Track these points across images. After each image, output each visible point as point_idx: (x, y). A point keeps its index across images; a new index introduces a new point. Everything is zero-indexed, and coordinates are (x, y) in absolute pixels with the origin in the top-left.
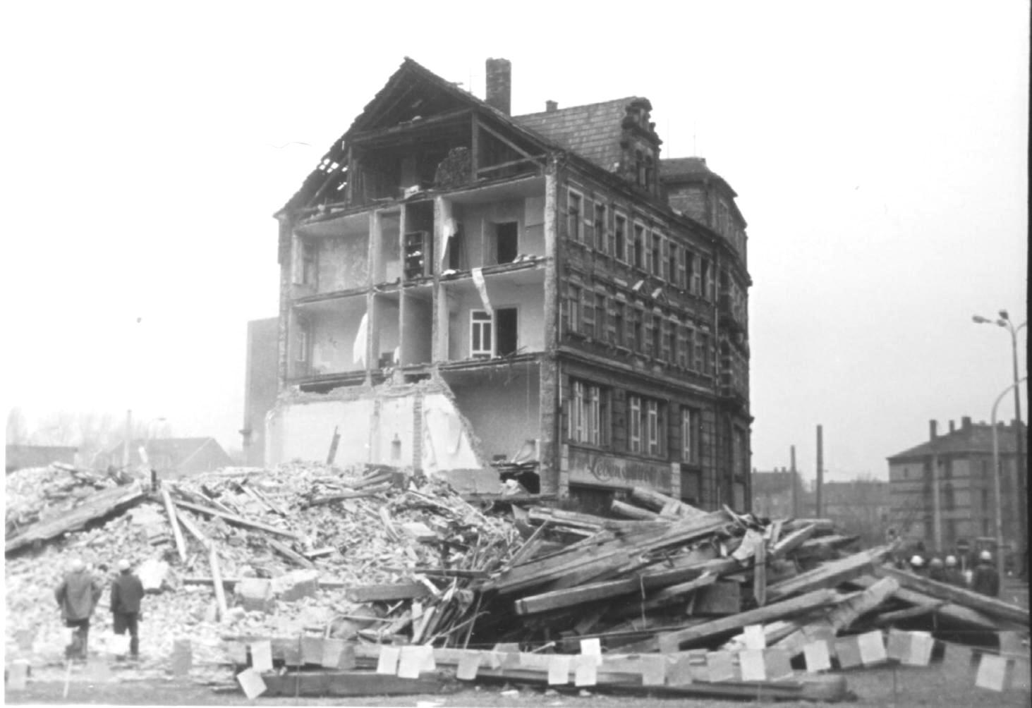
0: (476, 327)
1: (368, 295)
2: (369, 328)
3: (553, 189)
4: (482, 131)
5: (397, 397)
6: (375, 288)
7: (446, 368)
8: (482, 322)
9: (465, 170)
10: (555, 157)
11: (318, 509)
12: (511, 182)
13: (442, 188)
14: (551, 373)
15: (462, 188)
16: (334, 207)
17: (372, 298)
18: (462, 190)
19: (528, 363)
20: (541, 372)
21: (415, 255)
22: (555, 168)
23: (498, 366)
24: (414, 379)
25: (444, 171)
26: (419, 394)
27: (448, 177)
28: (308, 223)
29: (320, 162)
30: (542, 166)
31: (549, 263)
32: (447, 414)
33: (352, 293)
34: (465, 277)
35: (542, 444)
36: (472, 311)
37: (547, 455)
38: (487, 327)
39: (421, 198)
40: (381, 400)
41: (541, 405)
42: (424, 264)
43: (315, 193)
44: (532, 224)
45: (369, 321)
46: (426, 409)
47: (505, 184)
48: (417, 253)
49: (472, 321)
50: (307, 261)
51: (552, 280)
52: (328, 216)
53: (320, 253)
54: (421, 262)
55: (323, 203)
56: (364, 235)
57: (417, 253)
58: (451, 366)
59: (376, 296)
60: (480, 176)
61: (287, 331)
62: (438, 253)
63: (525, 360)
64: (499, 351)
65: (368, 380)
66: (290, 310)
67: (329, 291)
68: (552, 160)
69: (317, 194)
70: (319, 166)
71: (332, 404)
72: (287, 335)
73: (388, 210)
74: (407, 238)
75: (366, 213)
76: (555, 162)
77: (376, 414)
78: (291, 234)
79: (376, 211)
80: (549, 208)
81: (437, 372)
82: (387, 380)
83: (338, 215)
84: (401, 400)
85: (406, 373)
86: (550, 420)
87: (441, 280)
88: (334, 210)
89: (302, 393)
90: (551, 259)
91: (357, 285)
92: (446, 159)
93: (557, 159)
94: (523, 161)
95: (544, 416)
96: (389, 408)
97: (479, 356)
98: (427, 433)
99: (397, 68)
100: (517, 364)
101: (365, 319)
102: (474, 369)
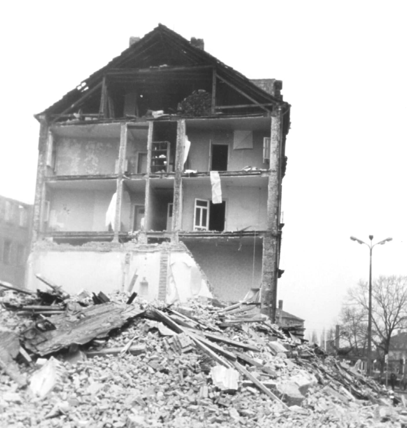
0: (198, 210)
1: (118, 180)
2: (118, 204)
3: (277, 126)
4: (218, 80)
5: (146, 252)
6: (124, 176)
7: (185, 236)
8: (202, 208)
9: (206, 105)
10: (280, 107)
11: (21, 318)
12: (244, 118)
13: (183, 114)
14: (273, 245)
15: (202, 117)
16: (88, 116)
17: (121, 183)
18: (203, 118)
19: (255, 237)
20: (263, 244)
21: (160, 157)
22: (279, 113)
23: (230, 237)
24: (152, 241)
25: (188, 104)
26: (164, 251)
27: (191, 108)
28: (64, 124)
29: (79, 84)
30: (268, 111)
31: (272, 173)
32: (190, 267)
33: (103, 177)
34: (203, 176)
35: (263, 292)
36: (196, 199)
37: (267, 299)
38: (205, 211)
39: (168, 119)
40: (131, 253)
41: (263, 266)
42: (167, 164)
43: (71, 105)
44: (239, 147)
45: (118, 199)
46: (172, 263)
47: (240, 118)
48: (162, 156)
49: (196, 207)
50: (54, 153)
51: (275, 185)
52: (82, 121)
53: (277, 120)
54: (165, 162)
55: (77, 112)
56: (116, 140)
57: (162, 156)
58: (190, 234)
59: (124, 182)
60: (218, 110)
61: (41, 199)
62: (180, 158)
63: (253, 235)
64: (211, 228)
65: (116, 240)
66: (44, 184)
67: (65, 174)
68: (277, 108)
69: (73, 106)
70: (77, 87)
71: (86, 253)
72: (41, 201)
73: (136, 124)
74: (154, 145)
75: (119, 123)
76: (280, 109)
77: (127, 263)
78: (47, 131)
79: (127, 123)
80: (273, 138)
81: (177, 238)
82: (132, 240)
83: (89, 123)
84: (149, 255)
85: (149, 236)
86: (269, 276)
87: (182, 176)
88: (87, 119)
89: (55, 244)
90: (274, 171)
91: (87, 173)
92: (190, 96)
93: (281, 108)
94: (253, 106)
95: (266, 273)
96: (138, 260)
97: (199, 229)
98: (171, 279)
99: (151, 29)
100: (245, 237)
101: (115, 196)
102: (209, 238)
